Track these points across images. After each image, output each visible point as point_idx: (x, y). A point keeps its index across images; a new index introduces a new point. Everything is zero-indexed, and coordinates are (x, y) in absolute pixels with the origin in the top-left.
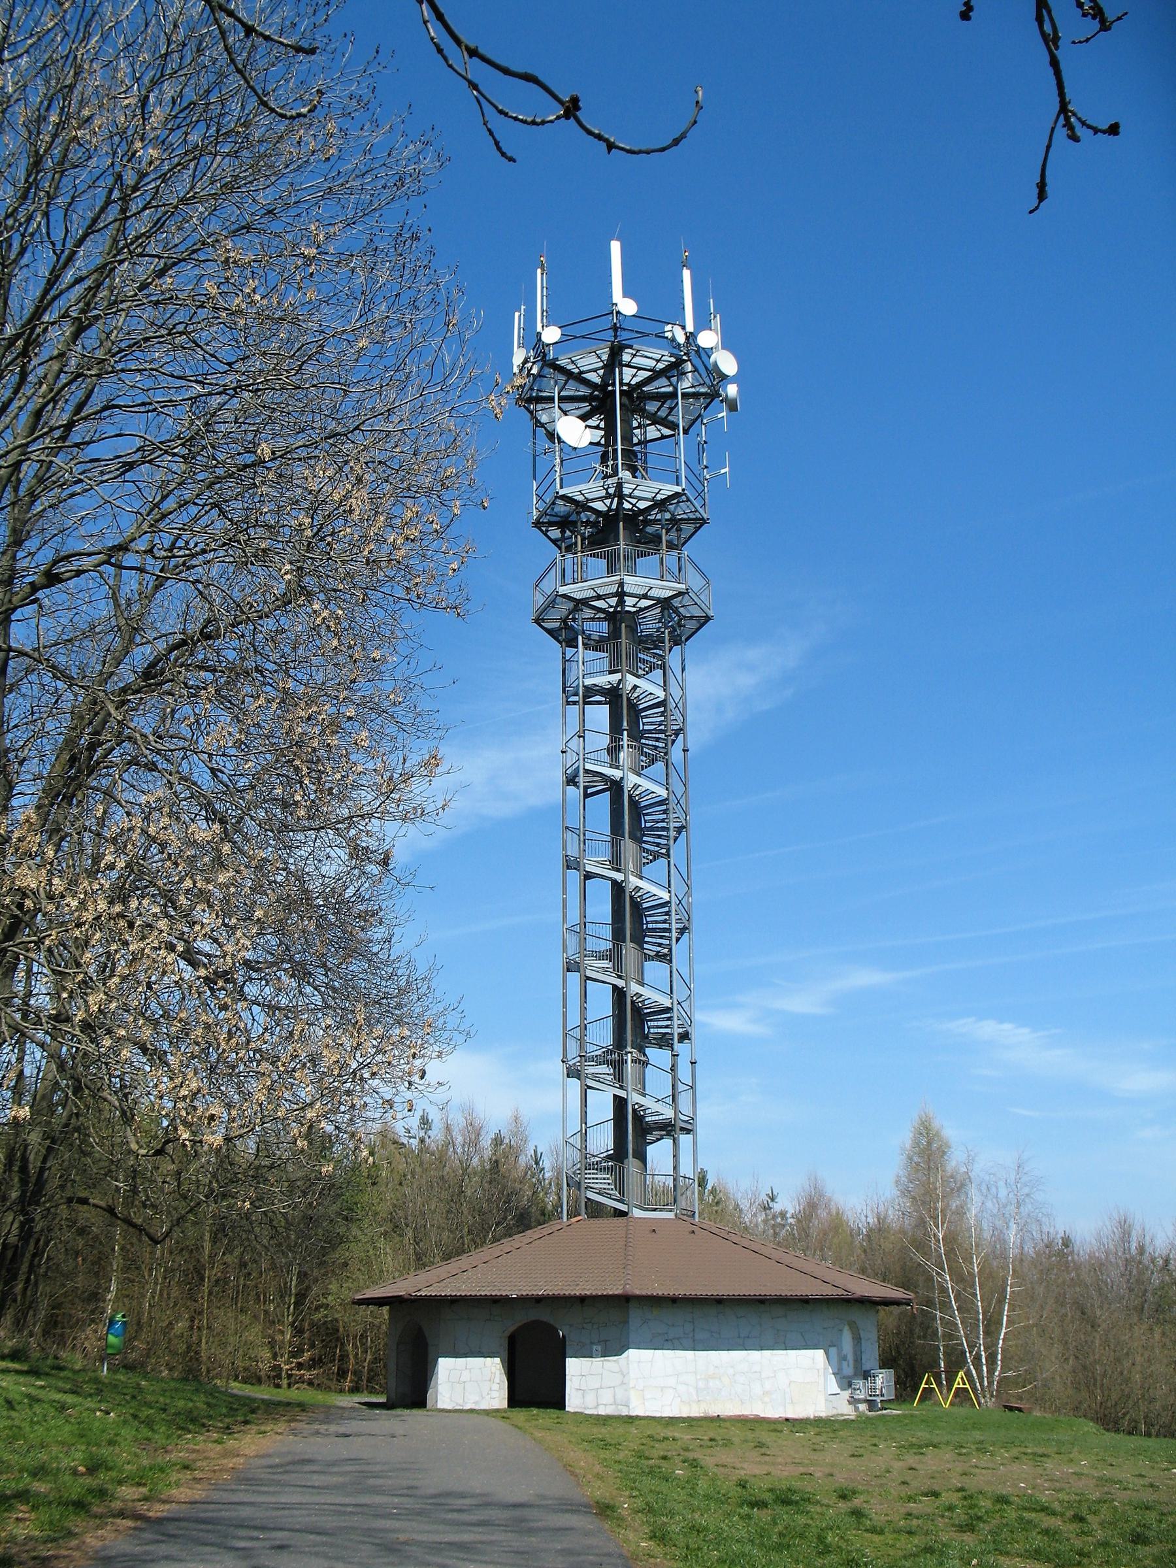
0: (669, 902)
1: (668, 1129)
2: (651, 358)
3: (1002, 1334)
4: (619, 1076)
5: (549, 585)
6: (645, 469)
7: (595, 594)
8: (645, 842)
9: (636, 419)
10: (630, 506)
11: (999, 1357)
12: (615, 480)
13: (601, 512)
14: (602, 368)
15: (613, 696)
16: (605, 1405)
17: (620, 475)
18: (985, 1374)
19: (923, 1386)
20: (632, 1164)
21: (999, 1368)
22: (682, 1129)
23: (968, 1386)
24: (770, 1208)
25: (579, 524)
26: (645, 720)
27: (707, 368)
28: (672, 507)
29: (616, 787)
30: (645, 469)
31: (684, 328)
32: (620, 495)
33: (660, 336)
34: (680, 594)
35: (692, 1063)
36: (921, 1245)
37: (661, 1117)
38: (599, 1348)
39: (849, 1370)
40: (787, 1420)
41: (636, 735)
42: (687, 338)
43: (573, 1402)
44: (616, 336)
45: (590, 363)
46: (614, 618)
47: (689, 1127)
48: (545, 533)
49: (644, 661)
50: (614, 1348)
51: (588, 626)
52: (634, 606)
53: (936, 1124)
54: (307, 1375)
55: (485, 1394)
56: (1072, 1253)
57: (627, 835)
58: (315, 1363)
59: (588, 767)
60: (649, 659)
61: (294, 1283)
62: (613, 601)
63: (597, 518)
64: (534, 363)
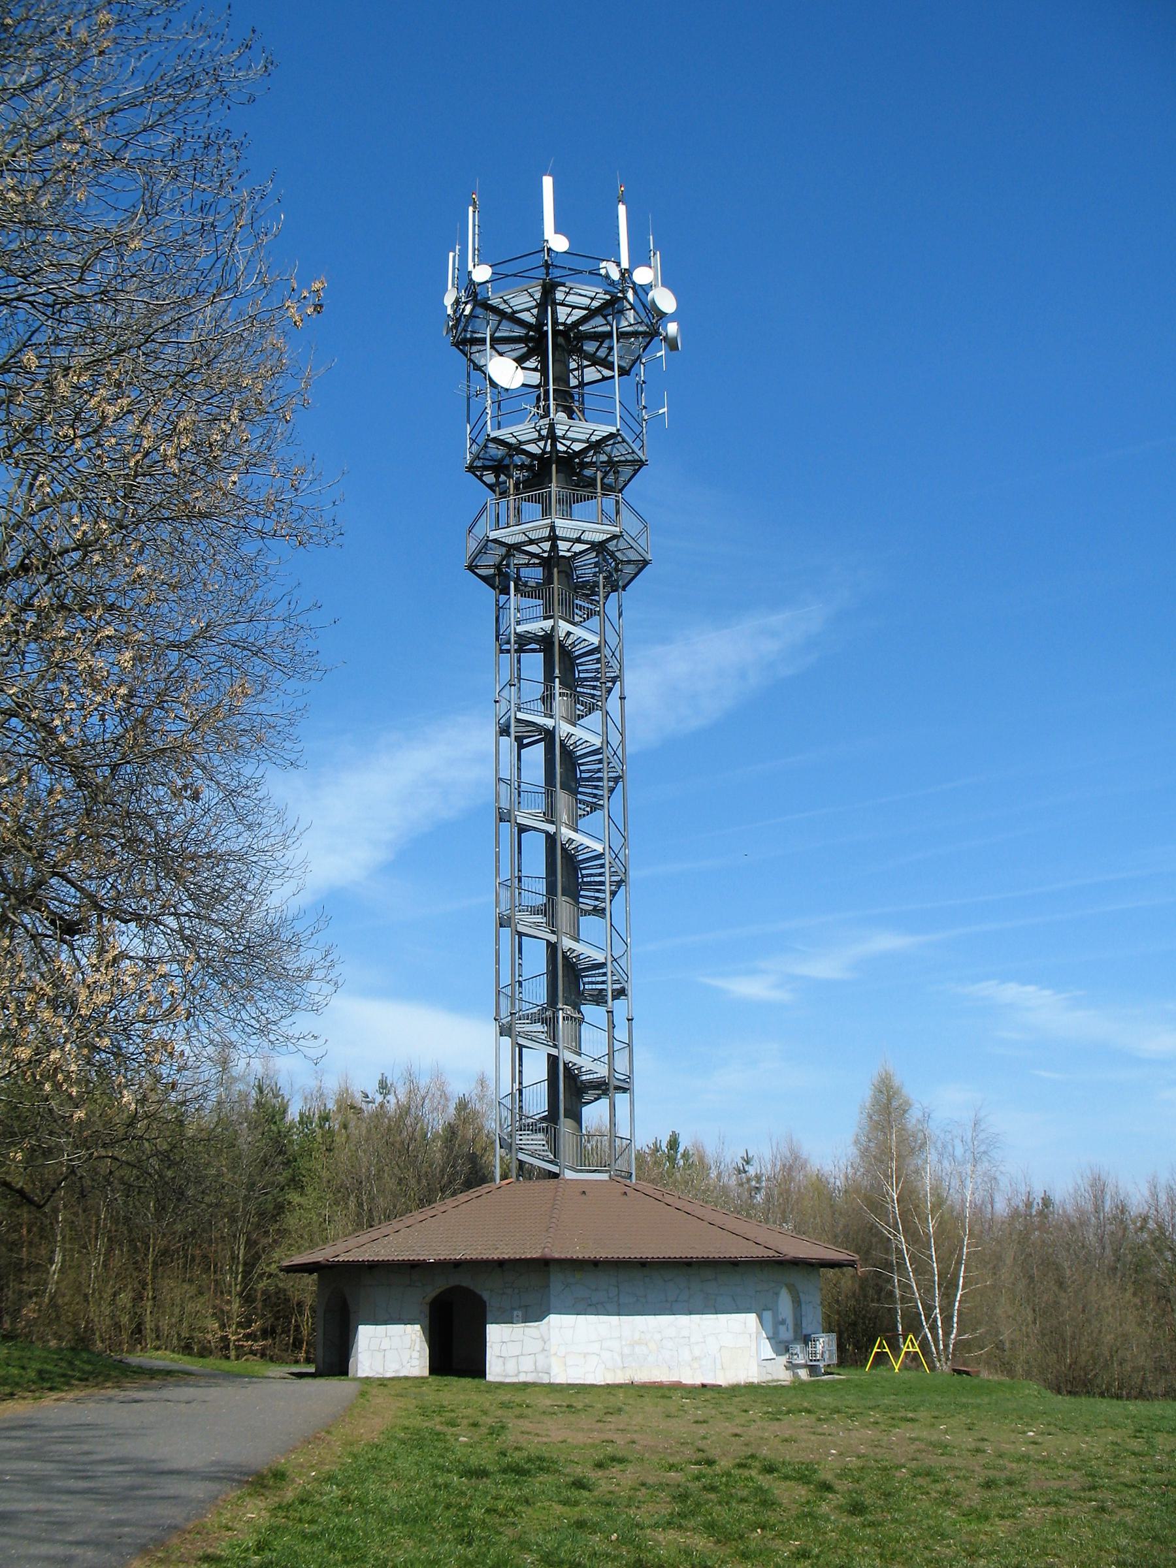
0: (603, 854)
1: (602, 1088)
2: (585, 296)
3: (959, 1296)
4: (553, 1036)
5: (482, 530)
6: (582, 411)
7: (527, 539)
8: (581, 793)
10: (565, 449)
11: (955, 1319)
12: (546, 421)
13: (535, 455)
14: (536, 307)
15: (546, 642)
16: (526, 1372)
17: (552, 416)
18: (941, 1337)
19: (875, 1350)
20: (566, 1126)
21: (955, 1331)
22: (618, 1088)
23: (918, 1350)
24: (745, 1172)
25: (512, 467)
26: (580, 668)
27: (644, 306)
28: (608, 449)
29: (549, 735)
30: (582, 411)
31: (618, 264)
32: (552, 437)
33: (595, 273)
34: (614, 537)
35: (628, 1020)
36: (877, 1205)
37: (595, 1076)
38: (520, 1314)
39: (786, 1334)
40: (704, 1386)
41: (571, 684)
42: (623, 275)
43: (495, 1370)
44: (547, 274)
45: (523, 301)
46: (550, 562)
47: (626, 1086)
48: (480, 478)
49: (581, 608)
50: (534, 1313)
51: (524, 572)
52: (568, 551)
53: (896, 1082)
54: (257, 1346)
55: (405, 1363)
56: (1053, 1213)
57: (558, 786)
58: (266, 1333)
59: (520, 716)
60: (587, 605)
61: (242, 1251)
62: (546, 546)
63: (532, 461)
64: (466, 303)
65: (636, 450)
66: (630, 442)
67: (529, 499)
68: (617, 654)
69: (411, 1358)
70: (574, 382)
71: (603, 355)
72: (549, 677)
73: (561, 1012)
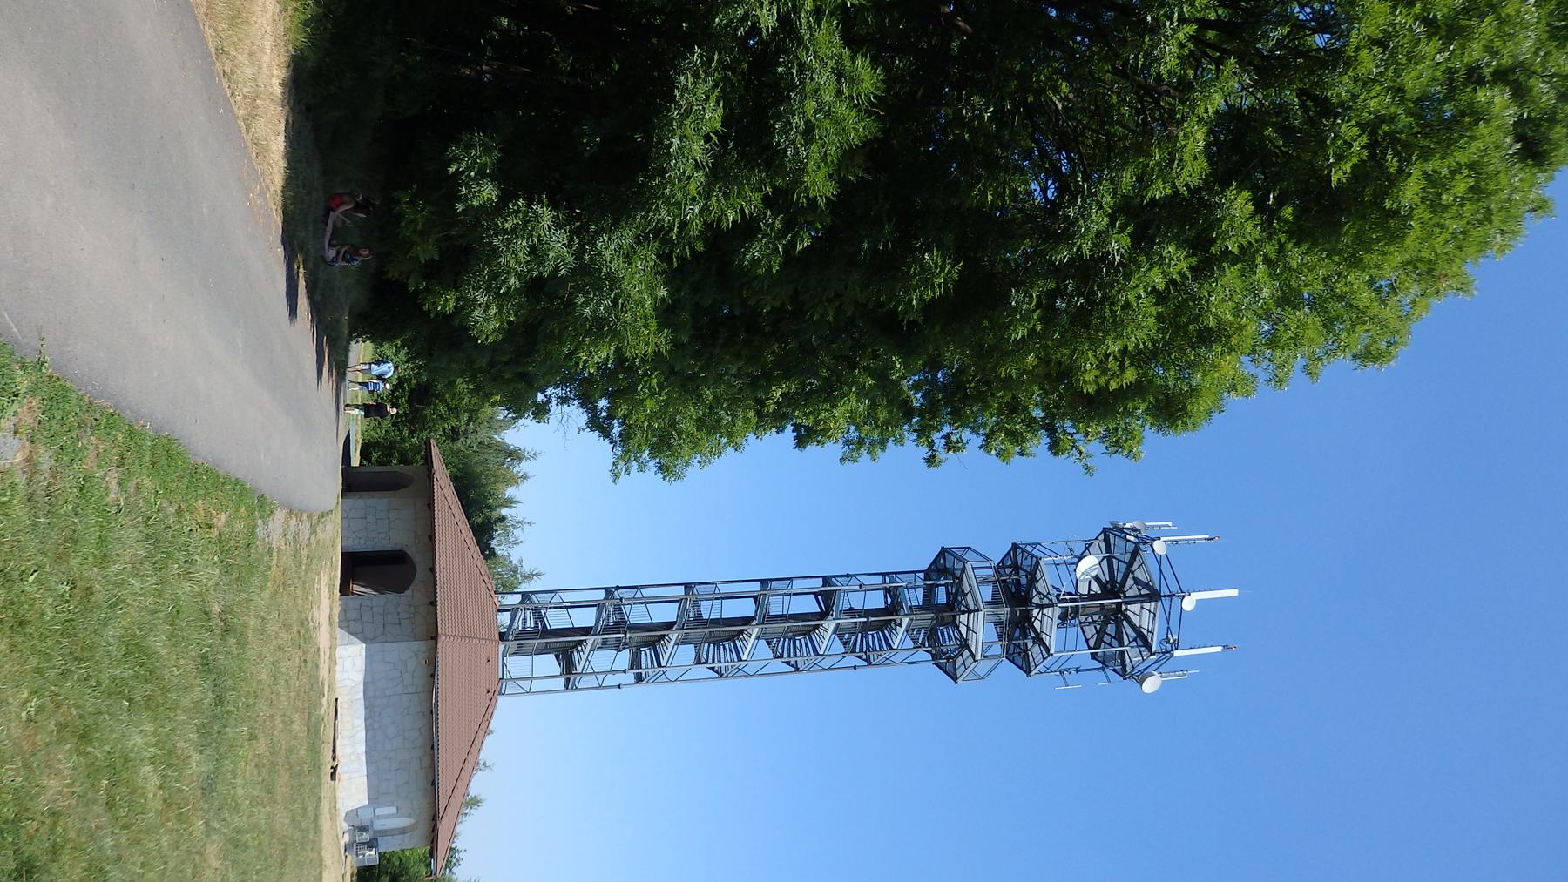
1: (569, 668)
4: (608, 629)
8: (785, 640)
9: (1100, 618)
17: (1059, 605)
22: (568, 681)
32: (1041, 607)
34: (973, 656)
37: (577, 662)
41: (865, 629)
47: (570, 687)
65: (1038, 668)
66: (1043, 664)
67: (995, 589)
68: (888, 662)
69: (360, 538)
70: (1082, 619)
71: (1105, 639)
72: (868, 613)
73: (623, 635)
